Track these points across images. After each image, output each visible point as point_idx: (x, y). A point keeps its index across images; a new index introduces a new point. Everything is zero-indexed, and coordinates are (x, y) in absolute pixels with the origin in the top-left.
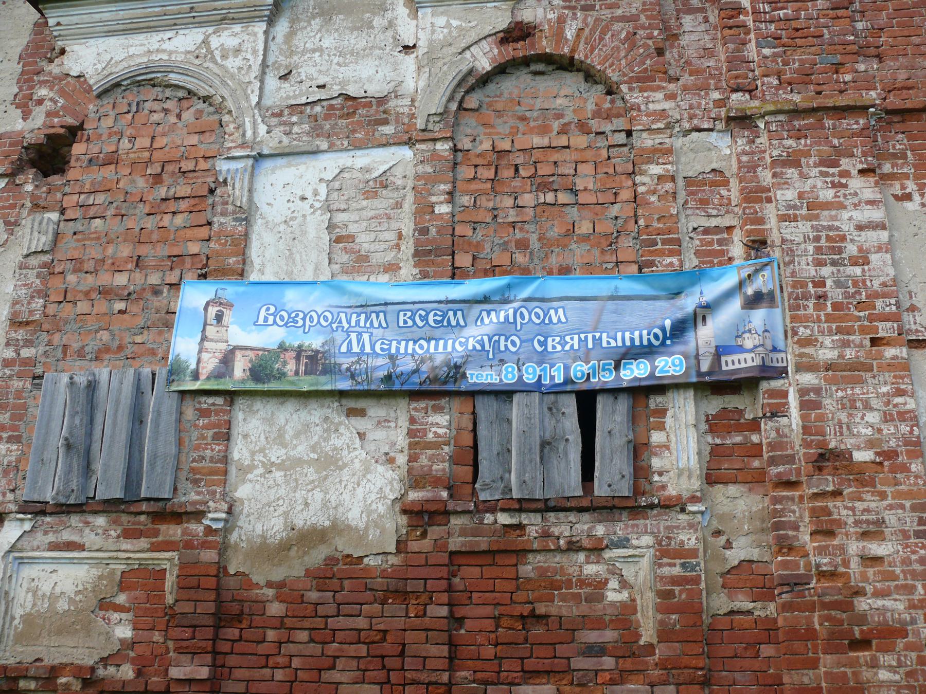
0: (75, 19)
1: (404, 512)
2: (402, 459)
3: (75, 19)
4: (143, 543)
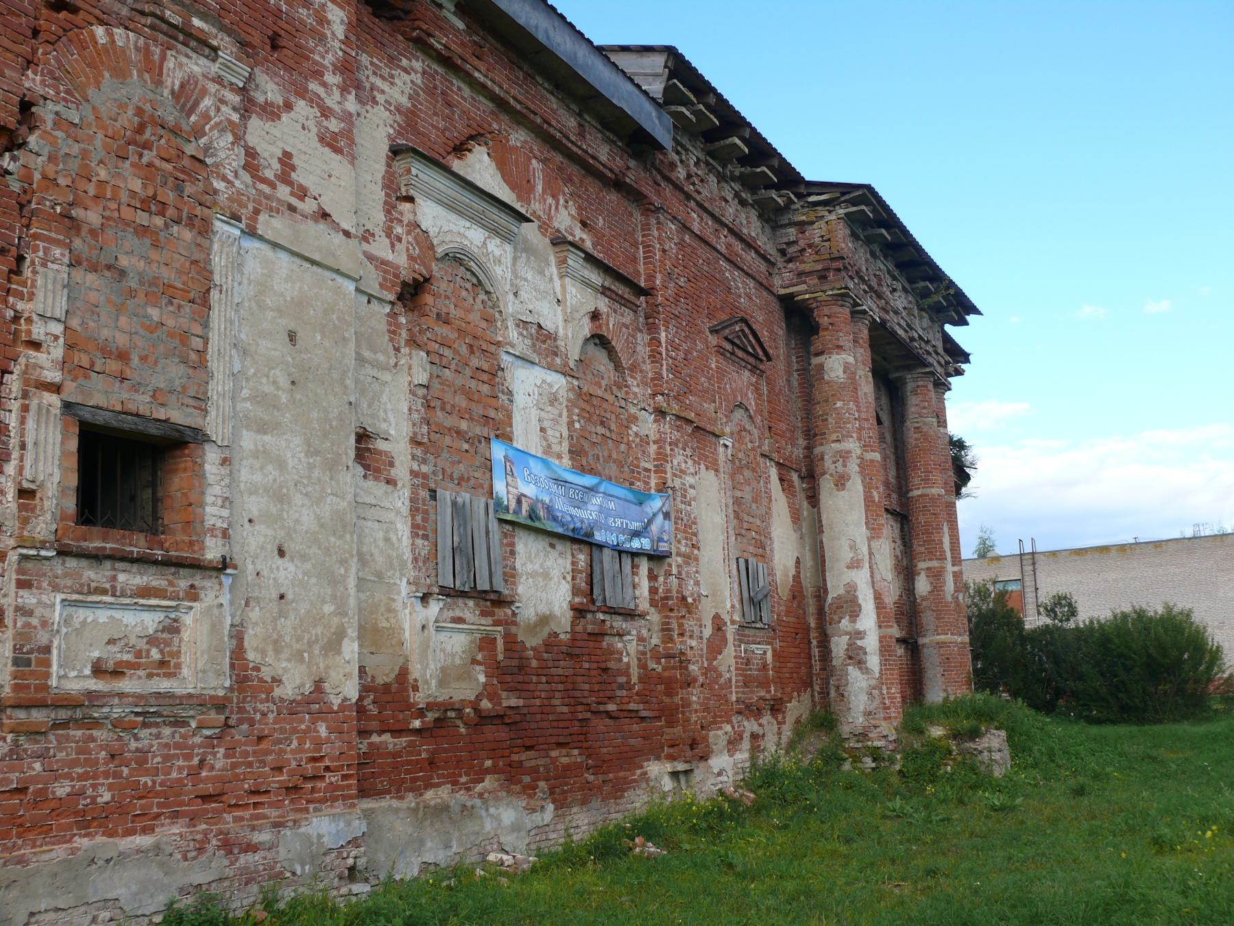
0: (425, 178)
1: (572, 609)
2: (569, 578)
3: (425, 178)
4: (489, 620)
